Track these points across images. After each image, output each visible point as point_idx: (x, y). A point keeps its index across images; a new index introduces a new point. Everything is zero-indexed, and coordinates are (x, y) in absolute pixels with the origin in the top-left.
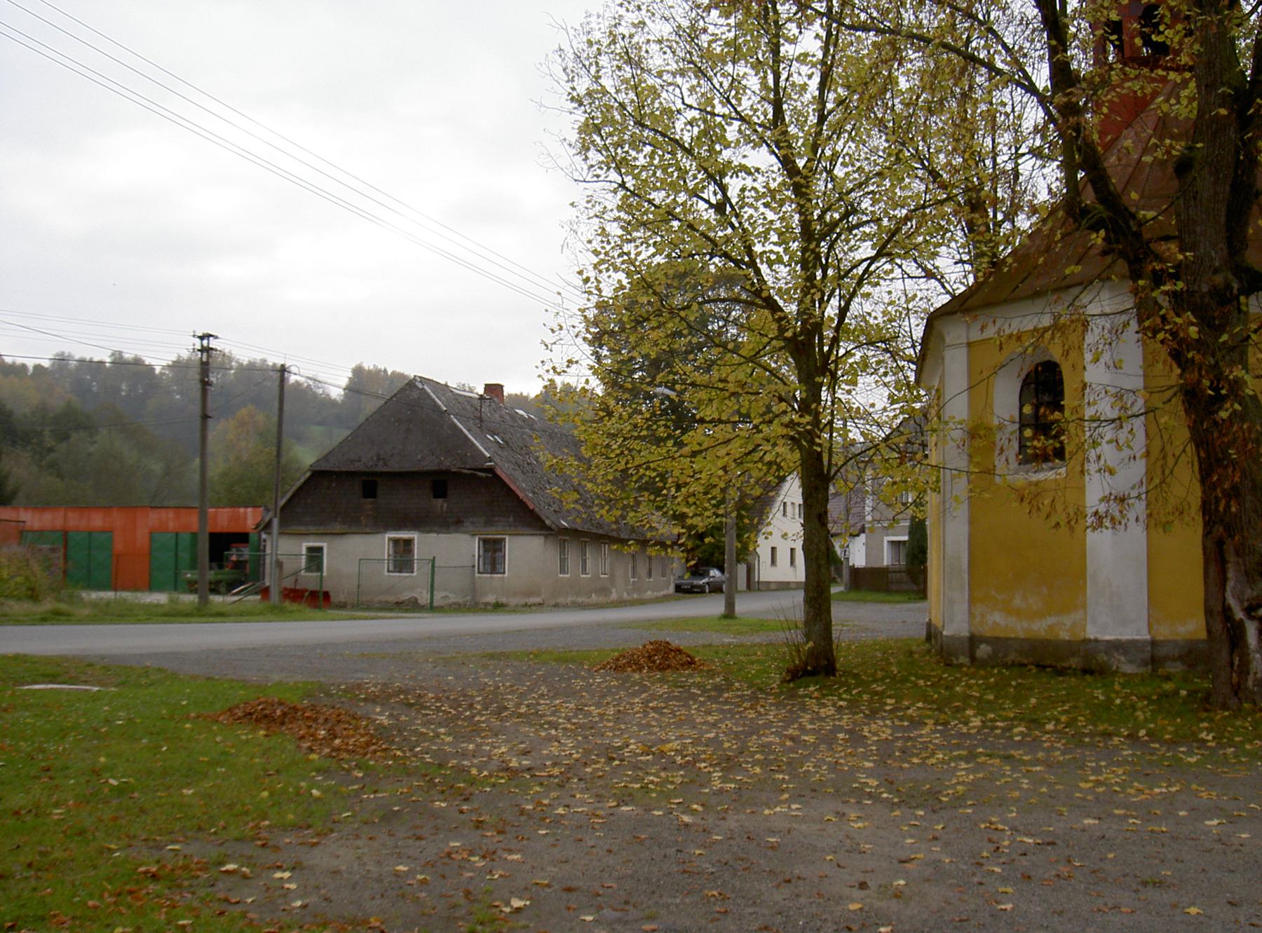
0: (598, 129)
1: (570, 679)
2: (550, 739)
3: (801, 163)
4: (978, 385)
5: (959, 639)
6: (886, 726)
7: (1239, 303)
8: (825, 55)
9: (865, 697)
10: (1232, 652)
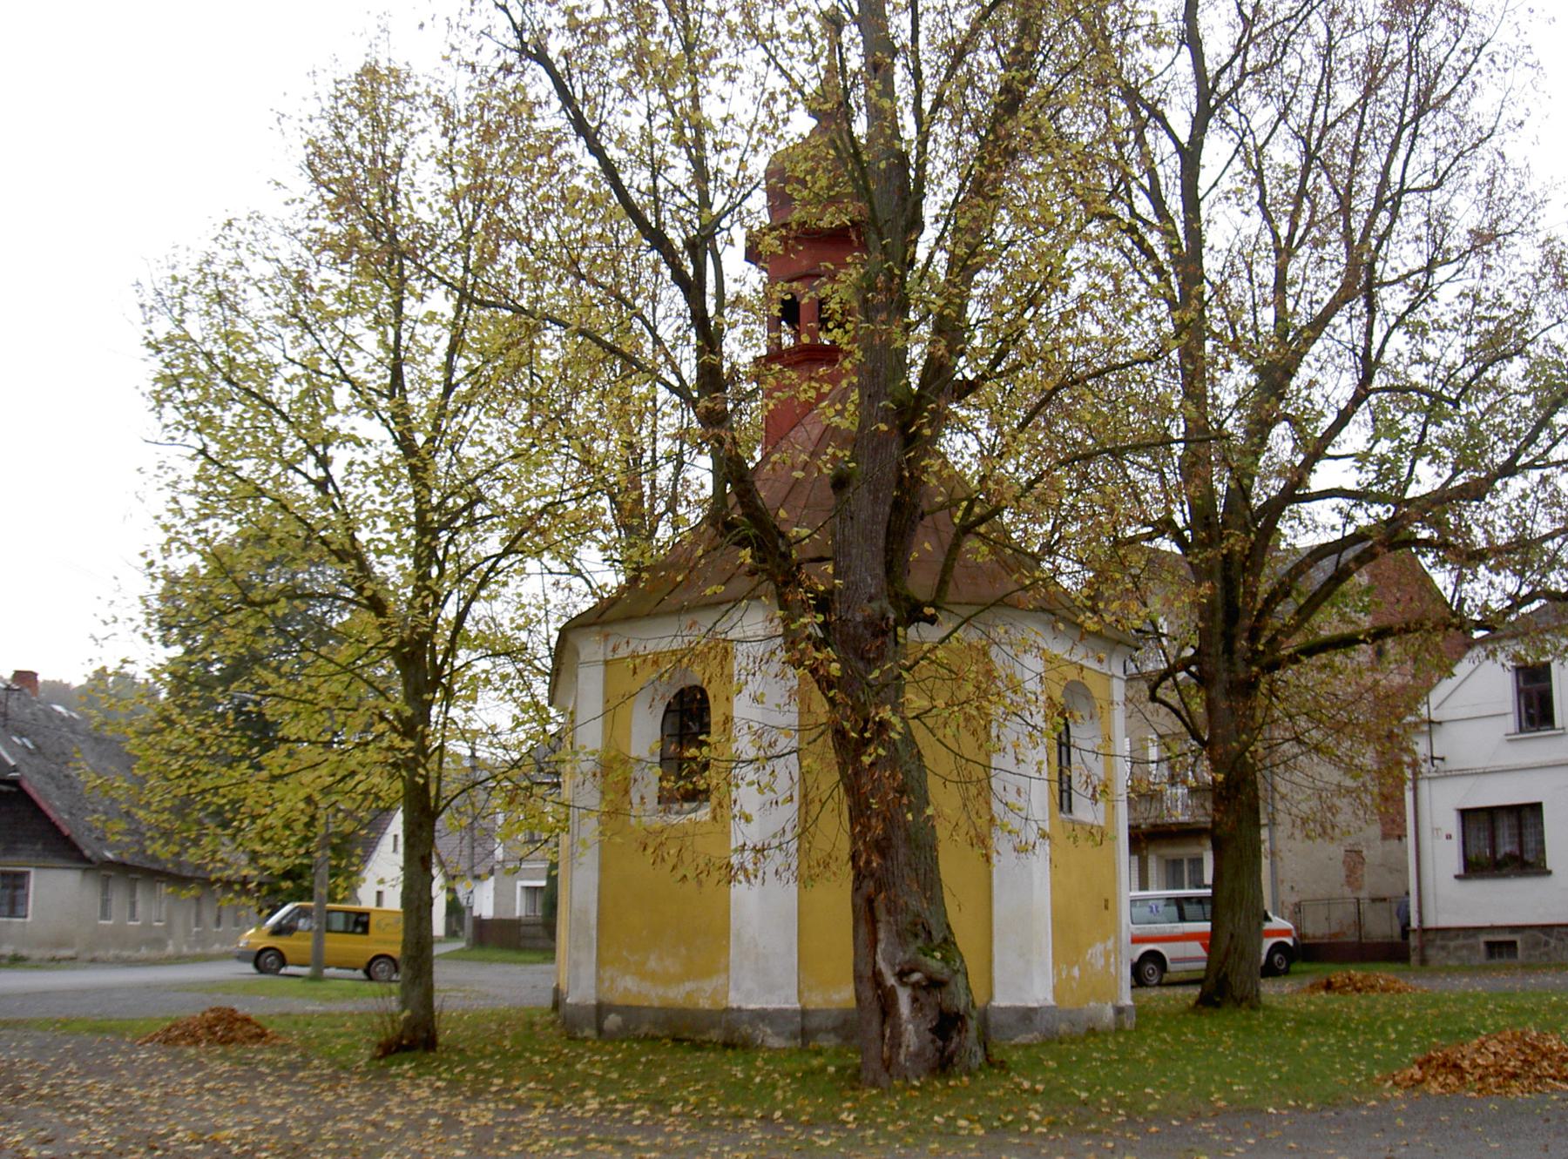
0: (176, 382)
1: (107, 1053)
2: (78, 1125)
3: (420, 439)
4: (613, 709)
5: (585, 1007)
6: (488, 1110)
7: (896, 634)
8: (457, 317)
9: (469, 1076)
10: (883, 1022)
